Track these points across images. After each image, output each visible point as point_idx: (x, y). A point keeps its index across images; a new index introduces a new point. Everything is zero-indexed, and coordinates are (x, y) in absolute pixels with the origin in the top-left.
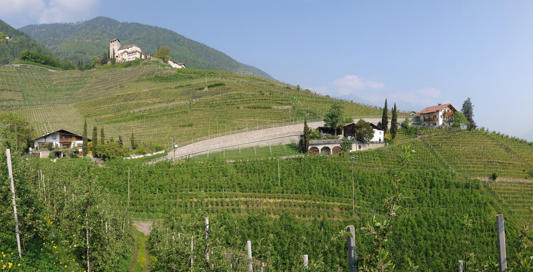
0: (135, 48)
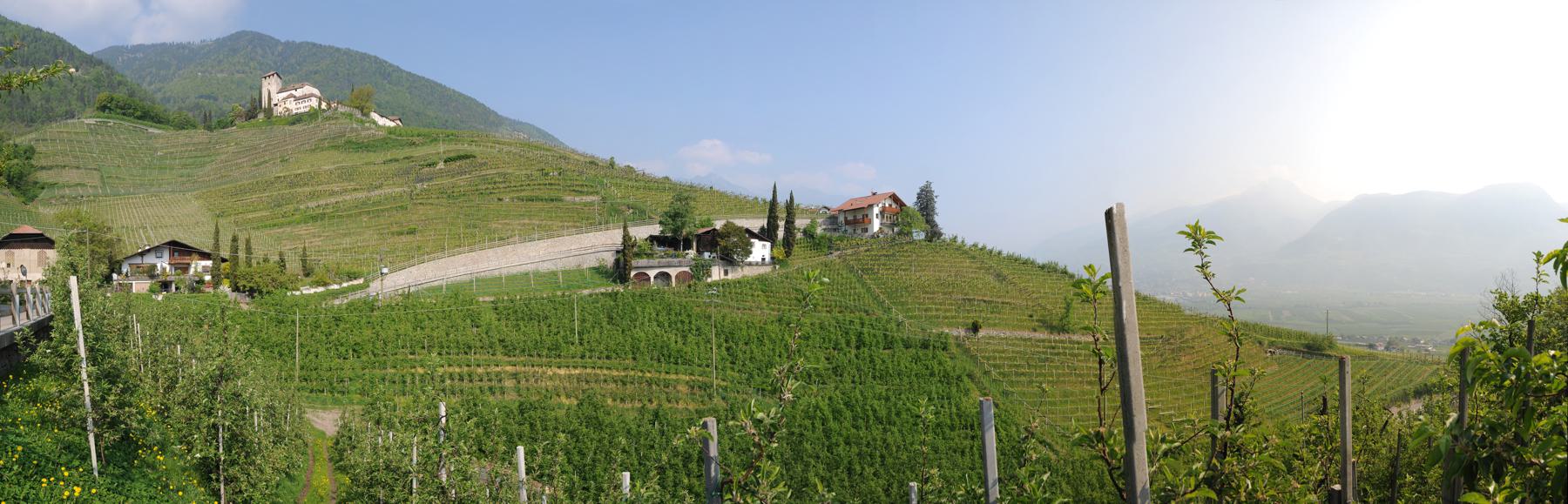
0: (308, 89)
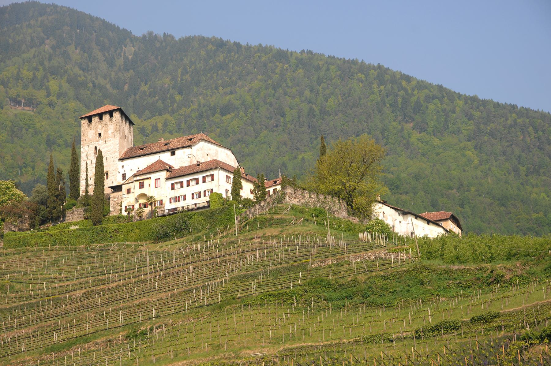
0: (204, 151)
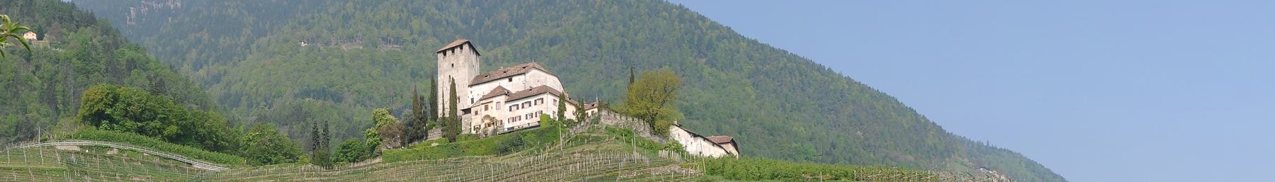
0: (536, 77)
